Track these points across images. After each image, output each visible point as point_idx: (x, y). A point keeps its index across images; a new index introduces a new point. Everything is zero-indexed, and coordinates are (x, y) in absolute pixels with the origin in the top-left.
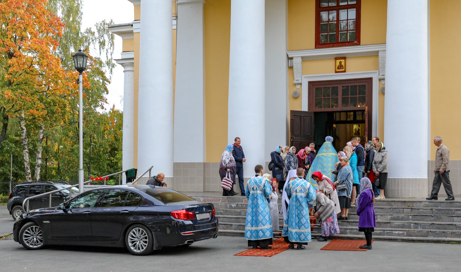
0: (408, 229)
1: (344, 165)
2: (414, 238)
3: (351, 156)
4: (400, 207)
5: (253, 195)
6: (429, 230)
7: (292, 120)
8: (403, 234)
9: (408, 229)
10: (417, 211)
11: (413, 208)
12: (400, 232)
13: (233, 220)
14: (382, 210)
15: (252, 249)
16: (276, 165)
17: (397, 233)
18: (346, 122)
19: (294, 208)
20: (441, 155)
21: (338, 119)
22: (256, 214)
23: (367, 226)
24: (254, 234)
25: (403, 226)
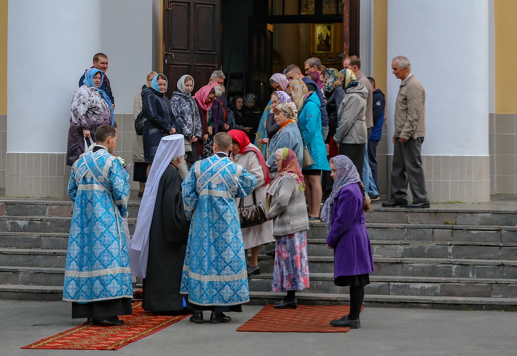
0: (444, 279)
1: (284, 124)
2: (460, 299)
3: (305, 103)
4: (426, 225)
5: (84, 193)
6: (493, 280)
7: (166, 11)
8: (434, 289)
9: (444, 279)
10: (465, 235)
11: (455, 226)
12: (427, 286)
13: (21, 258)
14: (384, 232)
15: (85, 324)
16: (153, 123)
17: (419, 287)
18: (297, 19)
19: (206, 225)
20: (406, 99)
21: (278, 12)
22: (88, 240)
23: (356, 271)
24: (84, 288)
25: (433, 271)
